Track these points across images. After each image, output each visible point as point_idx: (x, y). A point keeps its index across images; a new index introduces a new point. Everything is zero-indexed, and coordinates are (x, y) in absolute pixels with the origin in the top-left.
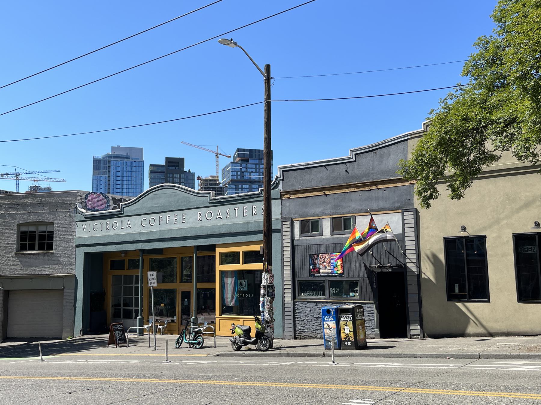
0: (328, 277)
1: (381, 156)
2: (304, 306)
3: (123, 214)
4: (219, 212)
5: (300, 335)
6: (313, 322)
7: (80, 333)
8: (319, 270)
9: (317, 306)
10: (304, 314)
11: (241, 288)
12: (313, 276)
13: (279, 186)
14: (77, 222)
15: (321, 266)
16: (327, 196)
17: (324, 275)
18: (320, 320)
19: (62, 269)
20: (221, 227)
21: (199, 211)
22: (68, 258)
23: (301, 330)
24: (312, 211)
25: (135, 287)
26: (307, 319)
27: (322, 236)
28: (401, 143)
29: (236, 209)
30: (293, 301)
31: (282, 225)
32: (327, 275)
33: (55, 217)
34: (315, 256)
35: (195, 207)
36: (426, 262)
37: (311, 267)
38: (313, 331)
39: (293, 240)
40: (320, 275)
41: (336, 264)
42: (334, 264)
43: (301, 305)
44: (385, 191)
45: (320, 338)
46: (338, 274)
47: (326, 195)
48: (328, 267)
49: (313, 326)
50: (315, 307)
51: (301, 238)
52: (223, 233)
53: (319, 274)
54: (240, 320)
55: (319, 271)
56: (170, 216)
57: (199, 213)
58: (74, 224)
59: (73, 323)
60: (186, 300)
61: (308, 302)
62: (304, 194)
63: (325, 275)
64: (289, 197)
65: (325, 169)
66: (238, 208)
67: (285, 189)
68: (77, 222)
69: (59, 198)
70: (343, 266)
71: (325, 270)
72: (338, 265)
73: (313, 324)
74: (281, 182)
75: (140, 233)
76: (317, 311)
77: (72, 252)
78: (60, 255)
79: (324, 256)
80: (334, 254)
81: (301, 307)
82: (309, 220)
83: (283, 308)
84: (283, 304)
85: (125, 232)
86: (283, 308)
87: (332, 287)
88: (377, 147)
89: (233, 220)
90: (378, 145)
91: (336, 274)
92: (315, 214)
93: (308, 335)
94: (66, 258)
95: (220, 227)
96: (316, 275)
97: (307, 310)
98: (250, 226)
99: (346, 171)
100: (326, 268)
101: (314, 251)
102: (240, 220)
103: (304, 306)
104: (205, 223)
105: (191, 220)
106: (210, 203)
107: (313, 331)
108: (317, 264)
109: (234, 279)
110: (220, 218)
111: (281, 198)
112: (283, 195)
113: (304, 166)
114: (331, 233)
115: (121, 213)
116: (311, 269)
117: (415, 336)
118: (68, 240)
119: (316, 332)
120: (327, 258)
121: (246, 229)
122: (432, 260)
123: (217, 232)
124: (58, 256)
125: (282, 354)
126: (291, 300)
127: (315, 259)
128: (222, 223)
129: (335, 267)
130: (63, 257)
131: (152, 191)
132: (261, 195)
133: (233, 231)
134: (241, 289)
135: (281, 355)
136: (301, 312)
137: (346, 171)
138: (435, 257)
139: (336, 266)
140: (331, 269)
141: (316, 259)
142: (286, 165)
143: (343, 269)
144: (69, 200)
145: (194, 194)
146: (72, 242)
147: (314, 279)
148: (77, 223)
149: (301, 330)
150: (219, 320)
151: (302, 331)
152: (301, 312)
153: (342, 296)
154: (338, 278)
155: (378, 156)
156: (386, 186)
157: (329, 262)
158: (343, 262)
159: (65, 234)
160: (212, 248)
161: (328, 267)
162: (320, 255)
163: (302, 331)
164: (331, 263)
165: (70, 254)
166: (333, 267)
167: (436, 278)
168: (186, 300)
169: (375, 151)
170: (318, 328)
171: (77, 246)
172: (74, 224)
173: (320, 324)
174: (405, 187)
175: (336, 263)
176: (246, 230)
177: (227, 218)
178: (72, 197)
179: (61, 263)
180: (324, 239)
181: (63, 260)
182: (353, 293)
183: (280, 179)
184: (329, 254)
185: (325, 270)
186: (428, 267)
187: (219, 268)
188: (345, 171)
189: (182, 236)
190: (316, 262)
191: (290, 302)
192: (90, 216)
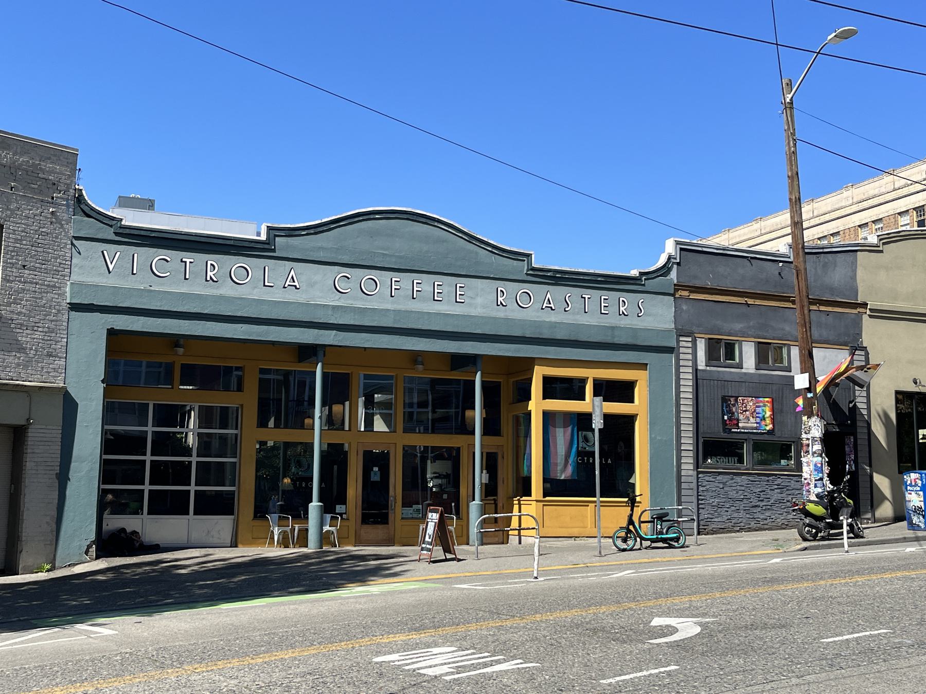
0: (751, 435)
1: (825, 265)
2: (713, 480)
3: (274, 251)
4: (549, 295)
5: (705, 527)
6: (727, 506)
7: (87, 553)
8: (738, 423)
9: (734, 481)
10: (713, 494)
11: (585, 446)
12: (727, 430)
13: (671, 273)
14: (77, 238)
15: (741, 417)
16: (749, 306)
17: (746, 431)
18: (738, 502)
19: (26, 367)
20: (555, 327)
21: (501, 285)
22: (46, 338)
23: (709, 520)
24: (727, 326)
25: (142, 438)
26: (717, 501)
27: (742, 368)
28: (850, 253)
29: (585, 298)
30: (696, 472)
31: (678, 341)
32: (750, 431)
33: (8, 209)
34: (732, 399)
35: (492, 276)
36: (877, 422)
37: (726, 417)
38: (728, 519)
39: (696, 371)
40: (739, 430)
41: (764, 416)
42: (760, 415)
43: (707, 478)
44: (828, 315)
45: (738, 531)
46: (766, 432)
47: (748, 305)
48: (751, 419)
49: (727, 511)
50: (730, 482)
51: (708, 368)
52: (559, 338)
53: (738, 429)
54: (588, 506)
55: (737, 425)
56: (425, 283)
57: (499, 289)
58: (66, 244)
59: (54, 526)
60: (376, 469)
61: (720, 473)
62: (714, 296)
63: (747, 431)
64: (689, 296)
65: (749, 264)
66: (589, 296)
67: (681, 280)
68: (77, 238)
69: (21, 155)
70: (773, 419)
71: (747, 423)
72: (766, 416)
73: (727, 509)
74: (675, 266)
75: (334, 307)
76: (734, 488)
77: (58, 323)
78: (21, 325)
79: (746, 401)
80: (761, 399)
81: (707, 481)
82: (721, 339)
83: (679, 483)
84: (679, 476)
85: (278, 295)
86: (679, 483)
87: (757, 451)
88: (821, 251)
89: (579, 316)
90: (823, 248)
91: (763, 430)
92: (732, 332)
93: (719, 527)
94: (38, 335)
95: (554, 325)
96: (733, 430)
97: (718, 487)
98: (617, 333)
99: (780, 274)
100: (749, 420)
101: (730, 391)
102: (591, 320)
103: (713, 480)
104: (513, 312)
105: (479, 300)
106: (527, 274)
107: (728, 519)
108: (736, 413)
109: (570, 429)
110: (551, 308)
111: (673, 295)
112: (678, 290)
113: (717, 249)
114: (706, 363)
115: (266, 246)
116: (726, 420)
117: (865, 521)
118: (48, 286)
119: (731, 522)
120: (751, 404)
121: (609, 338)
122: (883, 419)
123: (546, 334)
124: (13, 326)
125: (908, 538)
126: (693, 470)
127: (732, 404)
128: (553, 318)
129: (761, 420)
130: (28, 332)
131: (372, 217)
132: (638, 282)
133: (583, 338)
134: (585, 448)
135: (907, 540)
136: (707, 490)
137: (779, 273)
138: (886, 415)
139: (764, 419)
140: (757, 423)
141: (734, 405)
142: (688, 241)
143: (773, 423)
144: (52, 172)
145: (490, 249)
146: (59, 295)
147: (729, 436)
148: (75, 242)
149: (709, 520)
150: (544, 505)
151: (709, 520)
152: (707, 490)
153: (771, 465)
154: (766, 437)
155: (821, 264)
156: (830, 309)
157: (753, 410)
158: (773, 413)
159: (37, 265)
160: (528, 364)
161: (751, 419)
162: (740, 398)
163: (709, 520)
164: (757, 413)
165: (52, 326)
166: (759, 419)
167: (888, 445)
168: (376, 469)
169: (818, 255)
170: (736, 515)
171: (75, 307)
172: (66, 244)
173: (738, 508)
174: (853, 316)
175: (764, 413)
176: (609, 339)
177: (565, 311)
178: (63, 165)
179: (21, 349)
180: (745, 374)
181: (28, 339)
182: (786, 461)
183: (675, 261)
184: (754, 398)
185: (747, 423)
186: (879, 428)
187: (537, 405)
188: (778, 274)
189: (460, 330)
190: (734, 409)
191: (691, 473)
192: (143, 233)
